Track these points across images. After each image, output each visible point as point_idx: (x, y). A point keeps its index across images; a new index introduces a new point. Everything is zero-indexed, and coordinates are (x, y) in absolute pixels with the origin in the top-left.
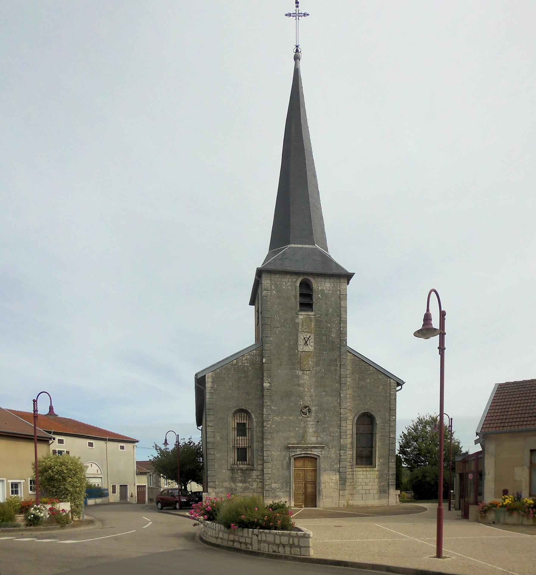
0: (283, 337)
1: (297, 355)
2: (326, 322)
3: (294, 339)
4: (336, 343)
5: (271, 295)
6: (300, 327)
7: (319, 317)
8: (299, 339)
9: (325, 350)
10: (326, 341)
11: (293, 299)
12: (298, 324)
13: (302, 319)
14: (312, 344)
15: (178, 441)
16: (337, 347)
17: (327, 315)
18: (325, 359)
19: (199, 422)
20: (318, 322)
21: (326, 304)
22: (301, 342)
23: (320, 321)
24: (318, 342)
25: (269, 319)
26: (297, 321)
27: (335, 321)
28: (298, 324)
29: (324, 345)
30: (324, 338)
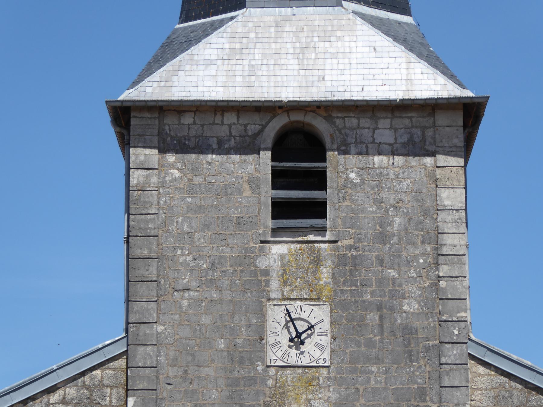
0: (205, 320)
1: (264, 381)
2: (381, 262)
3: (249, 326)
4: (421, 334)
5: (163, 184)
6: (275, 284)
7: (350, 247)
8: (271, 325)
9: (378, 361)
10: (381, 326)
11: (247, 193)
12: (266, 272)
13: (282, 257)
14: (325, 340)
15: (305, 115)
16: (427, 349)
17: (383, 237)
18: (375, 391)
19: (292, 7)
20: (348, 266)
21: (378, 202)
22: (277, 336)
23: (355, 262)
24: (346, 327)
25: (155, 263)
26: (262, 263)
27: (416, 257)
28: (266, 272)
29: (370, 344)
30: (372, 317)
